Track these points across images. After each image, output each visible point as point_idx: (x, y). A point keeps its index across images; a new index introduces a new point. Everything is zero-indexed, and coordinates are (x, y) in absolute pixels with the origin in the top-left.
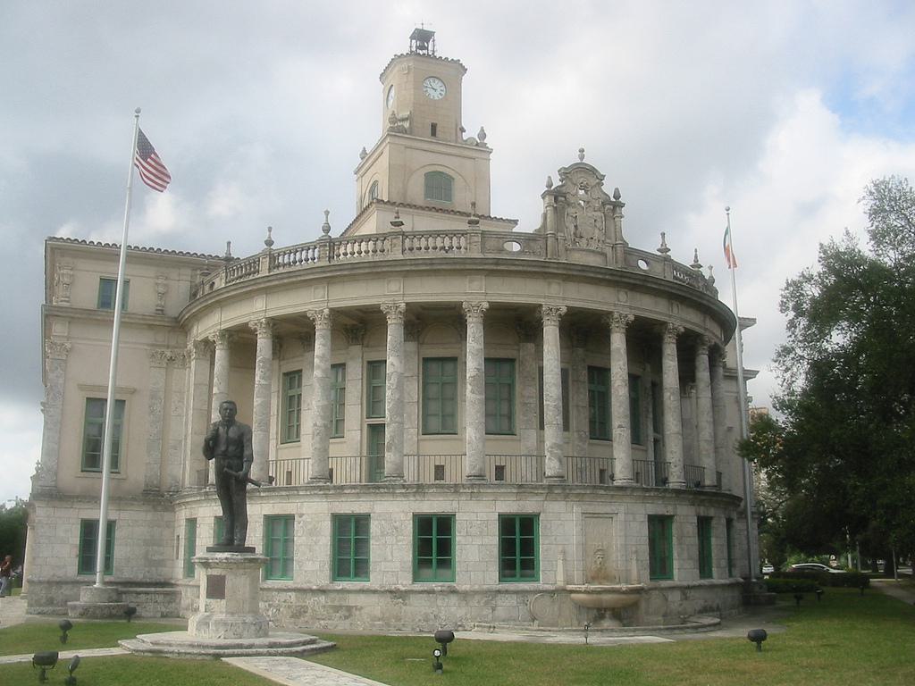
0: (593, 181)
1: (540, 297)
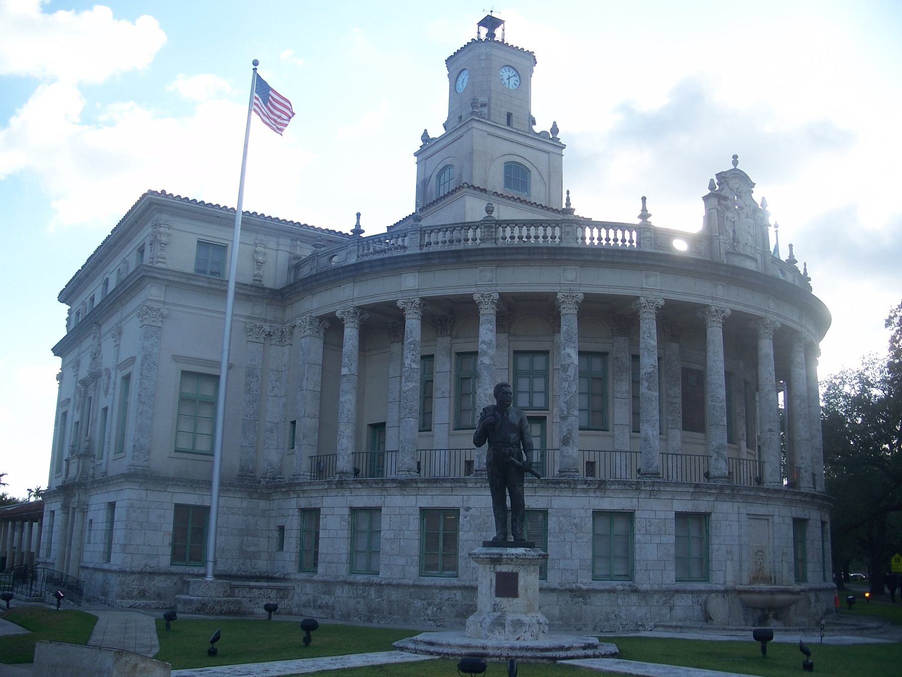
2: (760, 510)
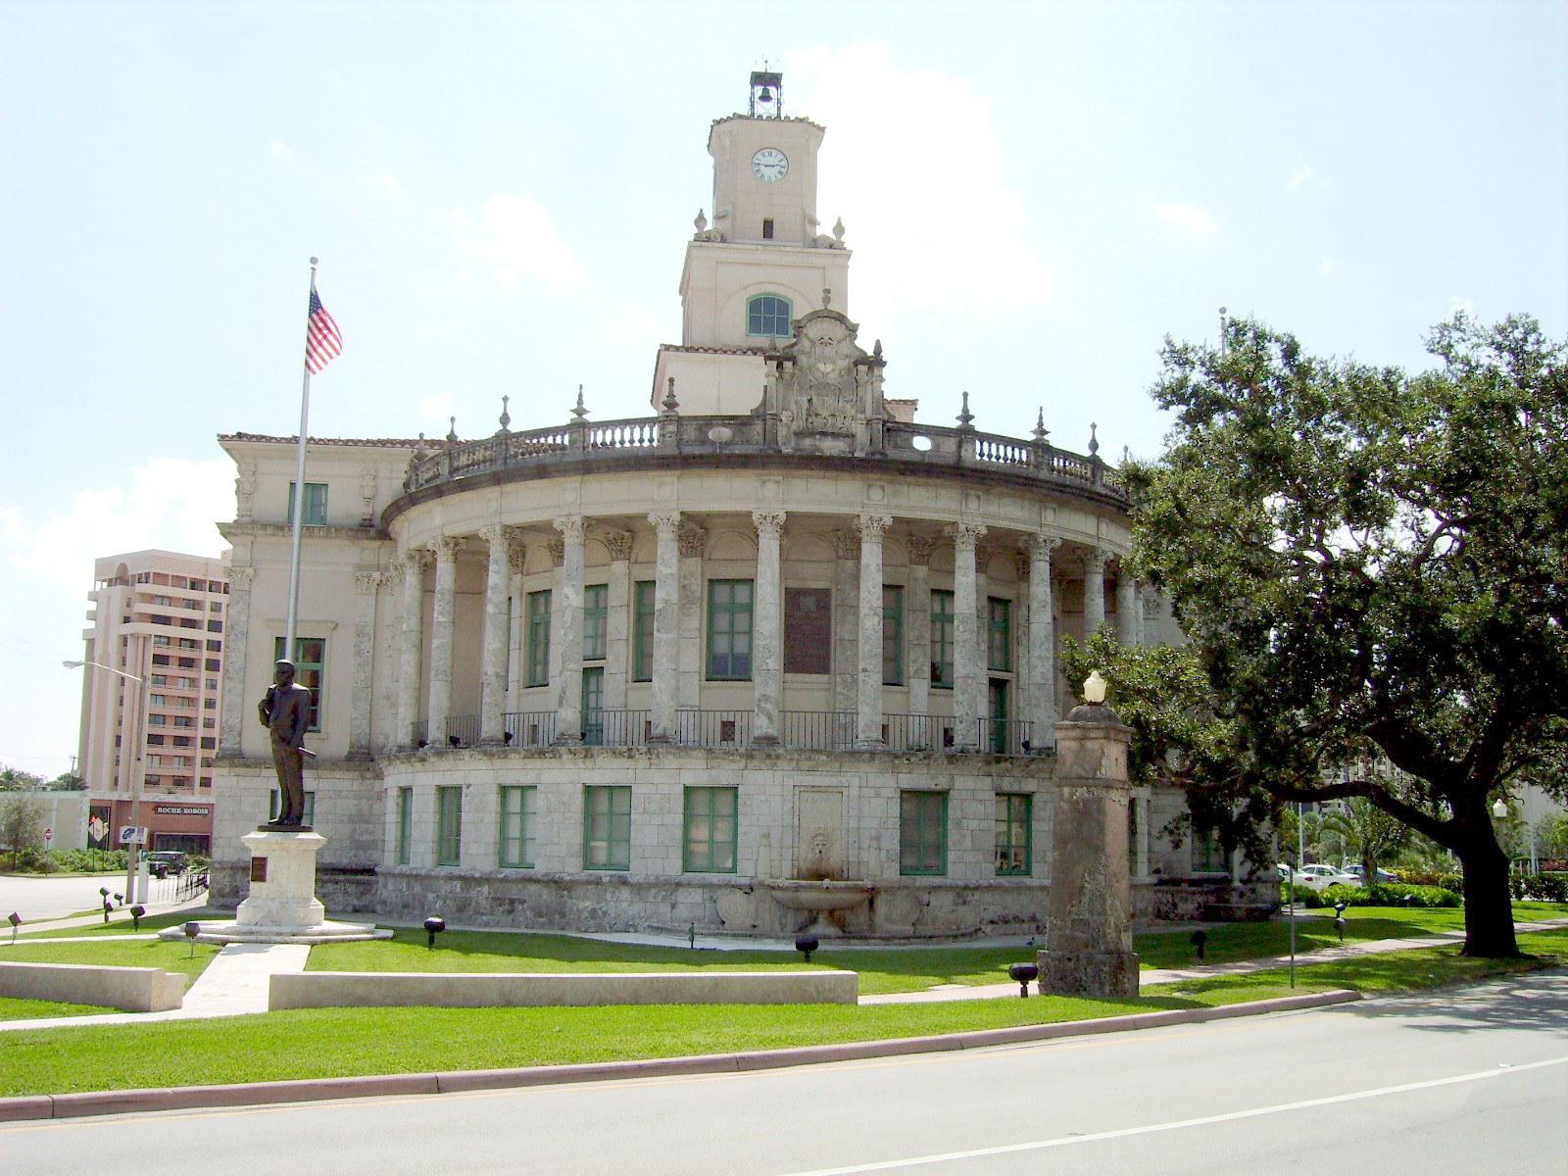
0: (839, 331)
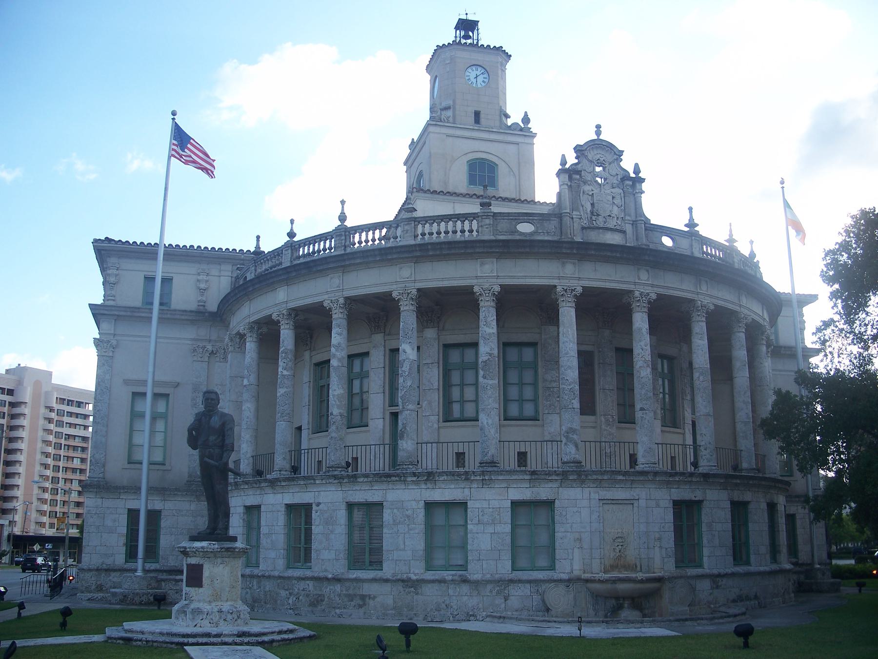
0: (609, 157)
1: (554, 278)
2: (620, 494)
